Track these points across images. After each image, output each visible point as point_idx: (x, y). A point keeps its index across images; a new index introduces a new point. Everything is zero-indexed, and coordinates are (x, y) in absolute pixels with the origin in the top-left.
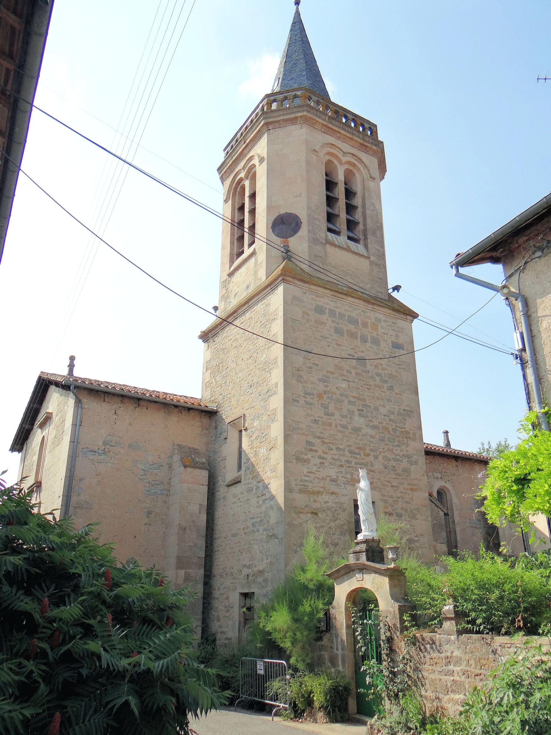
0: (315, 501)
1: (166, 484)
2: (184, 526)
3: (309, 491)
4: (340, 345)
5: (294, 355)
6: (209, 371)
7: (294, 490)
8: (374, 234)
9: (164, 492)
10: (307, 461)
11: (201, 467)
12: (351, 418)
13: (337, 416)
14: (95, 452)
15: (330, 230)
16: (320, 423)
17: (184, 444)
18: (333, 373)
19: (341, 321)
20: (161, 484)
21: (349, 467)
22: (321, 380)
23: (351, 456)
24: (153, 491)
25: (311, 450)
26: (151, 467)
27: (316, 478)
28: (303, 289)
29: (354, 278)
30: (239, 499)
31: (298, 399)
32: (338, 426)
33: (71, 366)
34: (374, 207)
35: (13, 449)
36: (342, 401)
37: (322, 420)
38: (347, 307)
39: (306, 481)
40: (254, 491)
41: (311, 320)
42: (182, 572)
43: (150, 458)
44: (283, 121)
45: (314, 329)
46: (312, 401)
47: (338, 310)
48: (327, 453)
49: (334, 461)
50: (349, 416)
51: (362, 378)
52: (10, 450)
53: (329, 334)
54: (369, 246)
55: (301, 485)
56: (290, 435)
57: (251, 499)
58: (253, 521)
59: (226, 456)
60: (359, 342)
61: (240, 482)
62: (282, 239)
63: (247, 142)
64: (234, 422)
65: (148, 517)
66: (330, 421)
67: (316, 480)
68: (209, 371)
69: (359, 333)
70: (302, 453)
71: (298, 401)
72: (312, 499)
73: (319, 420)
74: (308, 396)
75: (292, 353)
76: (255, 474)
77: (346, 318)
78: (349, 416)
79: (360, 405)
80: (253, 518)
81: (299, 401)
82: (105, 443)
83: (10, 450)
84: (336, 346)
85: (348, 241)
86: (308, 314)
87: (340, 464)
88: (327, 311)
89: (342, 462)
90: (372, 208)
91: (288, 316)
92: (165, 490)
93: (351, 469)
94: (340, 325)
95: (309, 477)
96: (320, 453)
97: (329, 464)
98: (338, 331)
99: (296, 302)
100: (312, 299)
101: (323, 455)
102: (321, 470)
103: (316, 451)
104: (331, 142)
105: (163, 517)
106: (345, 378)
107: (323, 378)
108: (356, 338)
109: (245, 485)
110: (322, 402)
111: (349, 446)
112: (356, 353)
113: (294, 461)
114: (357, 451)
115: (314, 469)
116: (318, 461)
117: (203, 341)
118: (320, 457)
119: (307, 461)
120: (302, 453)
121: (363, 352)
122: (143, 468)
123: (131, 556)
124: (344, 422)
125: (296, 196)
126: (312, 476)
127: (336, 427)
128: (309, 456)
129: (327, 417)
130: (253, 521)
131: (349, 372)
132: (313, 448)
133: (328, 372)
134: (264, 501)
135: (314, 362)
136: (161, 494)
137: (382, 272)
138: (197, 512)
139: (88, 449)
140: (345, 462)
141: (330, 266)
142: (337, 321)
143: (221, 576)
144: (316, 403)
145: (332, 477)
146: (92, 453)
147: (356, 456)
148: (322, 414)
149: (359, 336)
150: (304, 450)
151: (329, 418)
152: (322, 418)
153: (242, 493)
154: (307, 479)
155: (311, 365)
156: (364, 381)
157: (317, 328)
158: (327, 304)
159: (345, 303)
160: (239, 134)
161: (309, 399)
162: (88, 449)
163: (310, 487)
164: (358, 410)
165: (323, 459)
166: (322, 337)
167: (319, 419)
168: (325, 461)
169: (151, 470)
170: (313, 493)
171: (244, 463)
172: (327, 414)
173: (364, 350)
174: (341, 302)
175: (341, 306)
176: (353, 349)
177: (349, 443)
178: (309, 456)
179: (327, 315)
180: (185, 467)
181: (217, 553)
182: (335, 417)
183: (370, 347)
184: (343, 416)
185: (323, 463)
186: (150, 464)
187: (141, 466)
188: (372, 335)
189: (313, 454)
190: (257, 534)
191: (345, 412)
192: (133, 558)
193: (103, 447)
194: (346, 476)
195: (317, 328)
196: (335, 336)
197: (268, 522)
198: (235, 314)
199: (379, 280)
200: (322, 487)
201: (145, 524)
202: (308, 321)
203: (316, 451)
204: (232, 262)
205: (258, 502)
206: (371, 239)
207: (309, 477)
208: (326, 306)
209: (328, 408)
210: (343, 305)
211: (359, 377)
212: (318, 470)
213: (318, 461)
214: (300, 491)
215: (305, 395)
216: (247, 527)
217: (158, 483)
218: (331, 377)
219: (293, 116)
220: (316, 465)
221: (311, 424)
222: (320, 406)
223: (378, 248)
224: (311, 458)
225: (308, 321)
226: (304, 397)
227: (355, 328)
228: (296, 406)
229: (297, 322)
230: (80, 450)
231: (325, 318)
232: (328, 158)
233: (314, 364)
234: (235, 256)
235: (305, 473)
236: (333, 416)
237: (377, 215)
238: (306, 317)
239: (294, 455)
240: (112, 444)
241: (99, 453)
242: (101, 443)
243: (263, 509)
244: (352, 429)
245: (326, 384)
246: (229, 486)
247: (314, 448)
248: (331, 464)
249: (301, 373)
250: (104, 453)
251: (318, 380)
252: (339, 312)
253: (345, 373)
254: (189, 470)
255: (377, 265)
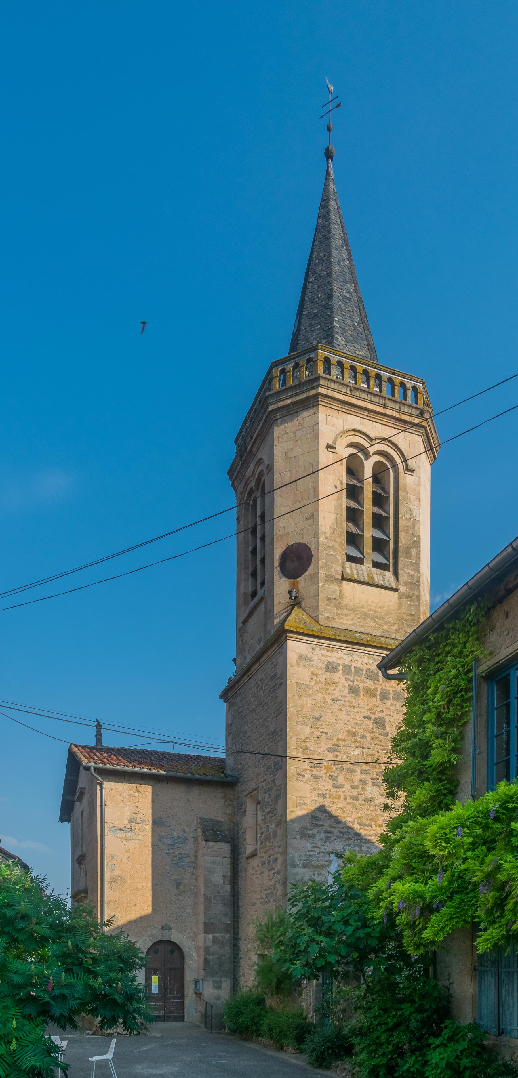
0: (319, 874)
1: (192, 856)
2: (209, 896)
3: (313, 865)
4: (354, 707)
5: (300, 724)
6: (231, 736)
7: (298, 865)
8: (408, 554)
9: (191, 864)
10: (313, 836)
11: (224, 840)
12: (363, 789)
13: (347, 786)
14: (122, 830)
15: (350, 559)
16: (327, 796)
17: (206, 817)
18: (344, 740)
19: (357, 678)
20: (187, 857)
21: (357, 840)
22: (329, 750)
23: (361, 828)
24: (180, 864)
25: (316, 825)
26: (177, 841)
27: (321, 852)
28: (311, 645)
29: (377, 620)
30: (256, 871)
31: (303, 773)
32: (348, 798)
33: (99, 736)
34: (411, 514)
35: (62, 820)
36: (355, 771)
37: (330, 793)
38: (366, 660)
39: (311, 856)
40: (266, 864)
41: (321, 681)
42: (210, 936)
43: (175, 833)
44: (293, 404)
45: (324, 692)
46: (318, 774)
47: (354, 665)
48: (334, 827)
49: (341, 835)
50: (361, 787)
51: (378, 743)
52: (60, 821)
53: (341, 696)
54: (400, 571)
55: (305, 860)
56: (294, 811)
57: (265, 872)
58: (266, 892)
59: (246, 829)
60: (378, 700)
61: (256, 855)
62: (291, 580)
63: (254, 439)
64: (251, 794)
65: (177, 888)
66: (338, 794)
67: (321, 854)
68: (231, 736)
69: (378, 689)
70: (307, 829)
71: (303, 776)
72: (316, 873)
73: (326, 794)
74: (314, 769)
75: (297, 724)
76: (267, 849)
77: (364, 673)
78: (361, 787)
79: (375, 773)
80: (266, 890)
81: (304, 775)
82: (131, 821)
83: (60, 821)
84: (348, 709)
85: (374, 570)
86: (317, 675)
87: (347, 837)
88: (340, 668)
89: (350, 834)
90: (408, 516)
91: (293, 681)
92: (192, 862)
93: (359, 841)
94: (356, 683)
95: (314, 851)
96: (326, 827)
97: (335, 838)
98: (353, 690)
99: (304, 662)
100: (322, 655)
101: (329, 829)
102: (327, 844)
103: (322, 826)
104: (354, 427)
105: (192, 887)
106: (358, 745)
107: (333, 747)
108: (375, 696)
109: (260, 858)
110: (331, 774)
111: (359, 818)
112: (374, 714)
113: (298, 837)
114: (367, 823)
115: (320, 843)
116: (323, 835)
117: (224, 701)
118: (326, 832)
119: (313, 836)
120: (307, 829)
121: (383, 711)
122: (169, 843)
123: (165, 923)
124: (355, 792)
125: (307, 519)
126: (317, 851)
127: (346, 799)
128: (314, 831)
129: (335, 789)
130: (266, 892)
131: (363, 737)
132: (318, 823)
133: (338, 739)
134: (274, 874)
135: (321, 730)
136: (189, 866)
137: (414, 606)
138: (221, 882)
139: (116, 828)
140: (354, 835)
141: (346, 609)
142: (352, 678)
143: (245, 940)
144: (324, 776)
145: (339, 851)
146: (119, 831)
147: (367, 828)
148: (330, 787)
149: (379, 693)
150: (309, 826)
151: (338, 789)
152: (330, 791)
153: (258, 866)
154: (312, 853)
155: (319, 734)
156: (381, 745)
157: (328, 689)
158: (341, 658)
159: (363, 654)
160: (244, 433)
161: (315, 772)
162: (116, 828)
163: (315, 861)
164: (372, 779)
165: (329, 833)
166: (333, 700)
167: (327, 792)
168: (331, 835)
169: (177, 845)
170: (318, 867)
171: (260, 837)
172: (335, 786)
173: (384, 709)
174: (358, 654)
175: (357, 659)
176: (369, 709)
177: (359, 815)
178: (314, 831)
179: (341, 672)
180: (207, 841)
181: (241, 919)
182: (344, 789)
183: (392, 705)
184: (352, 787)
185: (329, 837)
186: (176, 838)
187: (166, 841)
188: (395, 689)
189: (320, 828)
190: (269, 904)
191: (356, 782)
192: (166, 924)
193: (129, 825)
194: (354, 849)
195: (328, 689)
196: (349, 697)
197: (276, 894)
198: (249, 673)
199: (410, 617)
200: (327, 861)
201: (175, 895)
202: (317, 683)
203: (322, 826)
204: (246, 603)
205: (269, 875)
206: (402, 561)
207: (314, 851)
208: (339, 662)
209: (336, 780)
210: (361, 658)
211: (375, 742)
212: (323, 844)
213: (323, 835)
214: (304, 866)
215: (312, 769)
216: (262, 898)
217: (184, 856)
218: (342, 746)
219: (305, 395)
220: (321, 840)
221: (317, 798)
222: (327, 779)
223: (412, 572)
224: (316, 833)
225: (317, 683)
226: (310, 770)
227: (374, 683)
228: (301, 781)
229: (303, 686)
230: (108, 829)
231: (338, 676)
232: (352, 450)
233: (323, 732)
234: (250, 597)
235: (309, 849)
236: (342, 788)
237: (414, 526)
238: (315, 678)
239: (298, 831)
240: (137, 821)
241: (126, 831)
242: (126, 821)
243: (273, 882)
244: (363, 800)
245: (336, 753)
246: (249, 858)
247: (321, 823)
248: (337, 837)
249: (307, 744)
250: (131, 830)
251: (327, 750)
252: (355, 668)
253: (359, 739)
254: (210, 844)
255: (408, 597)
